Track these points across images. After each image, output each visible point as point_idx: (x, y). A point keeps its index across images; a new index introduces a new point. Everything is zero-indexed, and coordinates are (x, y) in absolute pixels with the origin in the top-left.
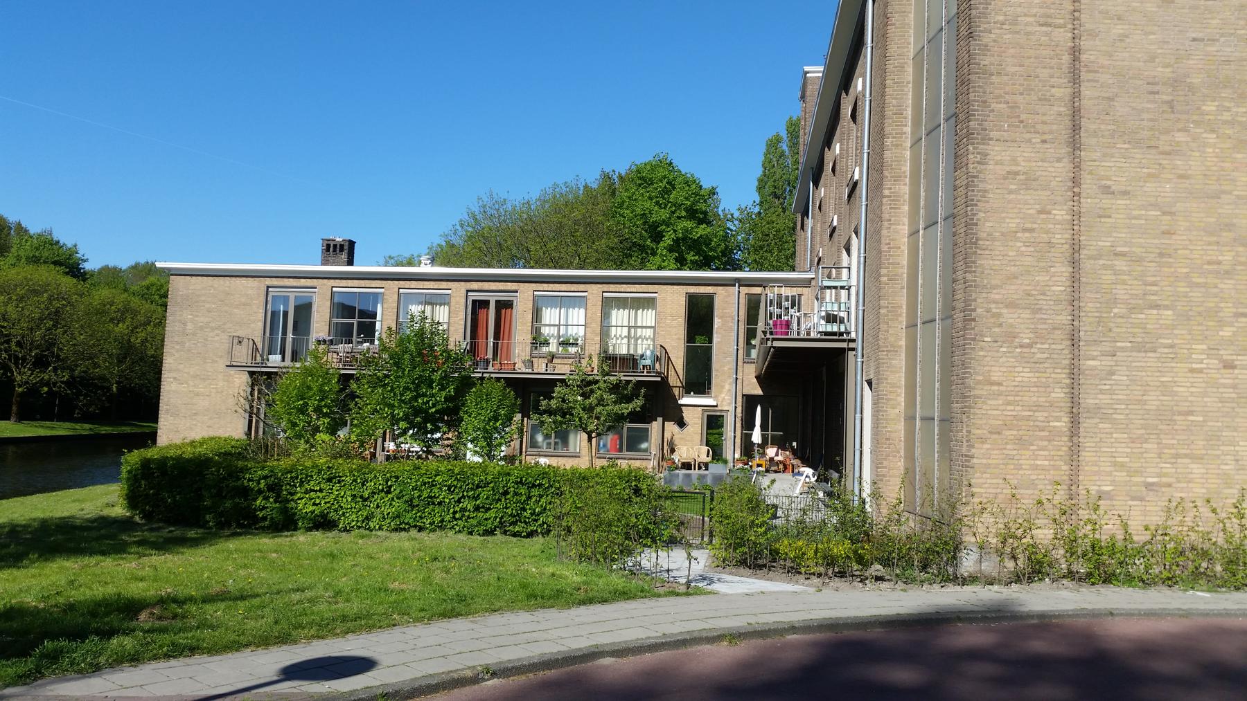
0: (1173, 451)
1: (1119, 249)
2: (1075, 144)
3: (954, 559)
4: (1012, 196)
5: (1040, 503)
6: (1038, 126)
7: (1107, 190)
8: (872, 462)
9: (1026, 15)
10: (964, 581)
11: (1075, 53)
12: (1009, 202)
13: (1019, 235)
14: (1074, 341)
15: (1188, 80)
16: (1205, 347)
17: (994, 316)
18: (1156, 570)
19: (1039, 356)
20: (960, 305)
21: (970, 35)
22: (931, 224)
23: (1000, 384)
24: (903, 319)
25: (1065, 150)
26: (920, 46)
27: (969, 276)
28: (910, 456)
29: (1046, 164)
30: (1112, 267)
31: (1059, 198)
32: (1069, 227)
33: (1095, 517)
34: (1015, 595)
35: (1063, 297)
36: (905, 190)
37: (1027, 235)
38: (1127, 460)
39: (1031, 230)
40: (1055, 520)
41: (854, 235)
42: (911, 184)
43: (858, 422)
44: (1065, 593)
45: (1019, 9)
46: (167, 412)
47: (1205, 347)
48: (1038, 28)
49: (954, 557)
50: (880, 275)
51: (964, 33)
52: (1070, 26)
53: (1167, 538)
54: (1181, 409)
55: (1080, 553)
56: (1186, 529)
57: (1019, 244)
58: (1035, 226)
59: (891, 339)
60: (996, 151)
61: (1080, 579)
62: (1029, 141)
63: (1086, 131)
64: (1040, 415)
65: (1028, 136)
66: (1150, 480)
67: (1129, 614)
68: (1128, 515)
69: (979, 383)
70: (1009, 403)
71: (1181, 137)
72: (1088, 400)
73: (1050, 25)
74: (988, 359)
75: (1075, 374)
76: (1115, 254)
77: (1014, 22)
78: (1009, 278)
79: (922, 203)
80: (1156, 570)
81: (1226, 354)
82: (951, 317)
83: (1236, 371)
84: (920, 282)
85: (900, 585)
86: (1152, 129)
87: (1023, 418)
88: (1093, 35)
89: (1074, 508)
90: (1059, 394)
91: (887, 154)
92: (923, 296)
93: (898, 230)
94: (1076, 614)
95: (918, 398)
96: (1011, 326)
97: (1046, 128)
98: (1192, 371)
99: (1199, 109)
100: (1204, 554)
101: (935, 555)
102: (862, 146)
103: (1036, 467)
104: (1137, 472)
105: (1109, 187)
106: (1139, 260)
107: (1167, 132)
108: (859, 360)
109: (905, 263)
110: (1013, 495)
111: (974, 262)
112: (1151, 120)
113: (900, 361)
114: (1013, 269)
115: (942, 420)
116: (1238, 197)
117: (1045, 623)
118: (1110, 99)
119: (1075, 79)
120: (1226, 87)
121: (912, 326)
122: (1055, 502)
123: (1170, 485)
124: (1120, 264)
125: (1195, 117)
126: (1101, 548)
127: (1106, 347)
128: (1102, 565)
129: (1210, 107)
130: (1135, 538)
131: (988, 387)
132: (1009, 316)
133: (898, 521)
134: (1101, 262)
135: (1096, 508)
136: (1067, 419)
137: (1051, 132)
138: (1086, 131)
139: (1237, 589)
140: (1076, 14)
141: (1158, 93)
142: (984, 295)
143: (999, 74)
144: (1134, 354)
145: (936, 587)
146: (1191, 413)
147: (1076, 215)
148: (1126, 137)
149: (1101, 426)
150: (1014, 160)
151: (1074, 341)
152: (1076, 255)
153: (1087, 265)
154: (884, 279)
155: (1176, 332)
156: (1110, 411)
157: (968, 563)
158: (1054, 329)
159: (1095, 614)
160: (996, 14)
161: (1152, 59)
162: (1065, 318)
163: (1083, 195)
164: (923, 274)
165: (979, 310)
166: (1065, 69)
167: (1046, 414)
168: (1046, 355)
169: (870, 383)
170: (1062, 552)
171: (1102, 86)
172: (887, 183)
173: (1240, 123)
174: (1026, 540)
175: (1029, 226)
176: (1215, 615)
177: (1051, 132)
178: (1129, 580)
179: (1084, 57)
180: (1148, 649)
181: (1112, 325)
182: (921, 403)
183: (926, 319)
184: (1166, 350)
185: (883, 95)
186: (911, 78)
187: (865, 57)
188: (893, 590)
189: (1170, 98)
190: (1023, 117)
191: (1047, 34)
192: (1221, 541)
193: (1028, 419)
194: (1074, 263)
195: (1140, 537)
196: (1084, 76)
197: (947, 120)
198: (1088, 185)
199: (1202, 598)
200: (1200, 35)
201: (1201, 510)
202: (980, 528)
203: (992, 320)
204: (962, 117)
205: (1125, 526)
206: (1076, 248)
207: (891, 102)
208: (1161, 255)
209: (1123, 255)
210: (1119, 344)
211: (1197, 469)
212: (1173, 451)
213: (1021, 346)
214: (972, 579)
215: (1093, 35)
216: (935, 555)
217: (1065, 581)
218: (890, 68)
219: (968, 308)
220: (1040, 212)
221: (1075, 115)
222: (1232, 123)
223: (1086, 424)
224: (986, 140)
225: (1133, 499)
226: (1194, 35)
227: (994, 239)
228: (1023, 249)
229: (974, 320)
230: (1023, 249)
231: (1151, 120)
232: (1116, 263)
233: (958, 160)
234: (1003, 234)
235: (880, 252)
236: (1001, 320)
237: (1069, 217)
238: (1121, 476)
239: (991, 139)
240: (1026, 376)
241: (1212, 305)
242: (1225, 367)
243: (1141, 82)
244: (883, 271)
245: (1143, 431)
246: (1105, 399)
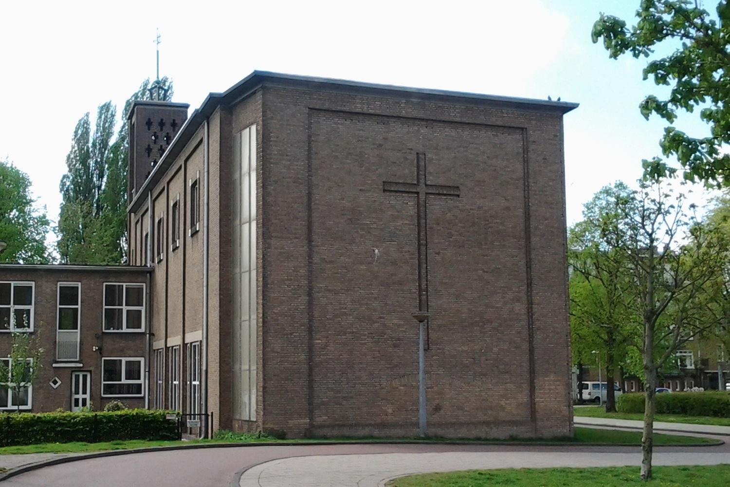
2: (310, 240)
98: (361, 344)
141: (345, 214)
238: (331, 393)
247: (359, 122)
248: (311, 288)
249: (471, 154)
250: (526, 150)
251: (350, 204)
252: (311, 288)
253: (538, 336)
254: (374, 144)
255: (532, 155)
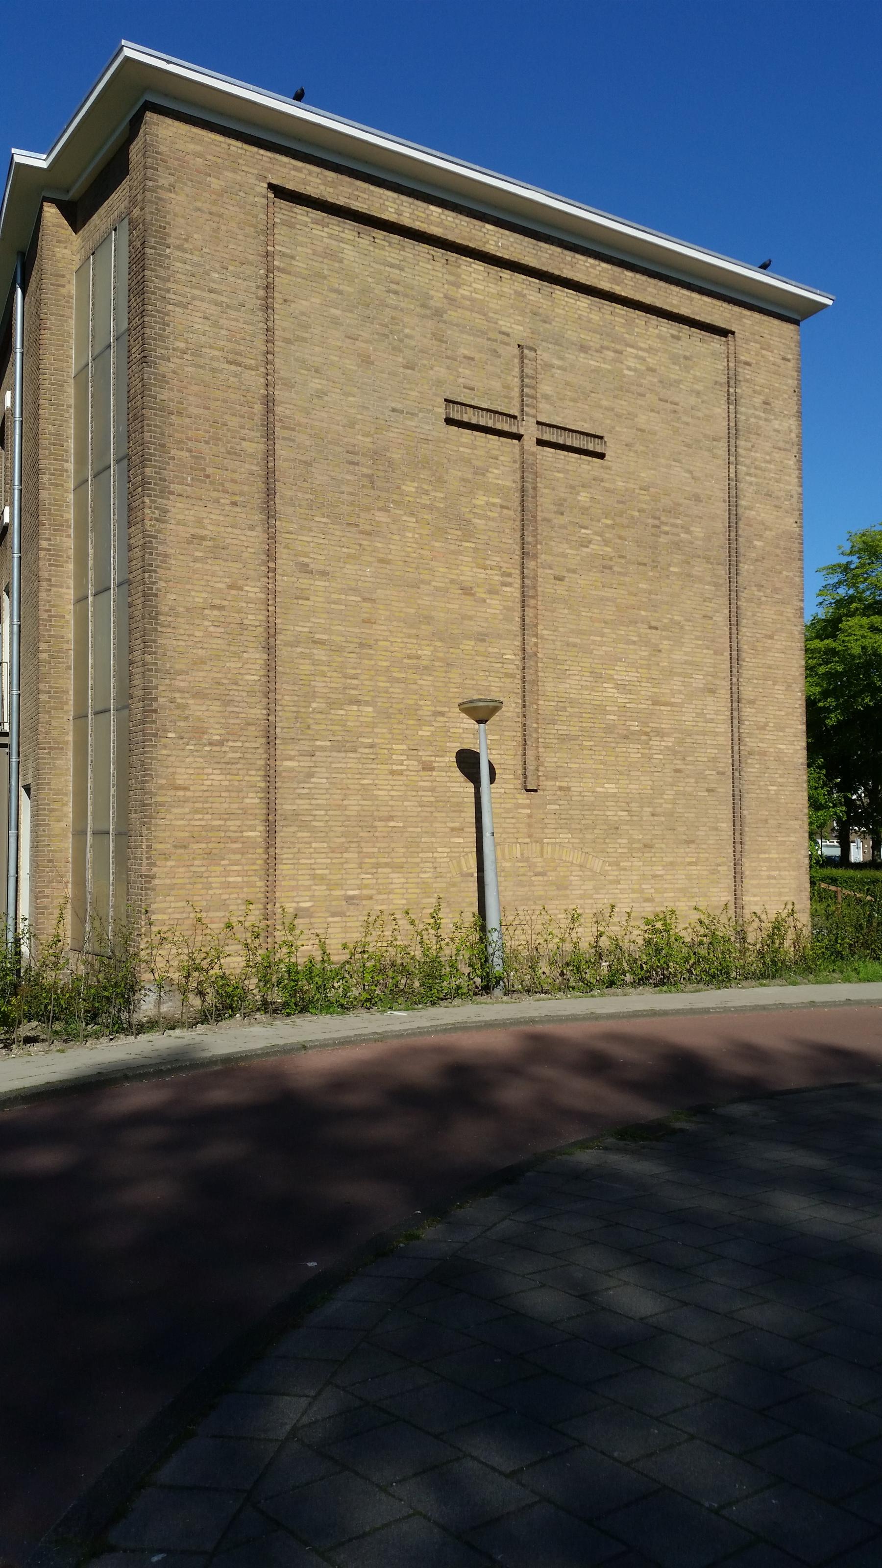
0: (374, 860)
1: (317, 636)
2: (269, 512)
3: (128, 1004)
4: (198, 565)
5: (229, 926)
6: (227, 485)
7: (304, 568)
8: (31, 891)
9: (211, 347)
10: (141, 1029)
11: (269, 403)
12: (195, 572)
13: (206, 612)
14: (270, 739)
15: (388, 454)
16: (404, 747)
17: (180, 707)
18: (355, 992)
19: (231, 755)
20: (138, 693)
21: (144, 360)
22: (102, 590)
23: (186, 789)
24: (70, 707)
25: (258, 517)
26: (83, 363)
27: (148, 657)
28: (80, 882)
29: (236, 531)
30: (310, 657)
31: (252, 573)
32: (263, 607)
33: (291, 938)
34: (198, 1039)
35: (257, 688)
36: (69, 543)
37: (216, 612)
38: (327, 871)
39: (221, 608)
40: (247, 945)
41: (5, 596)
42: (76, 537)
43: (13, 840)
44: (256, 1030)
45: (203, 338)
46: (472, 904)
47: (404, 747)
48: (226, 366)
49: (128, 1002)
50: (38, 650)
51: (136, 355)
52: (263, 370)
53: (366, 956)
54: (381, 814)
55: (274, 979)
56: (385, 944)
57: (207, 623)
58: (226, 603)
59: (55, 733)
60: (177, 508)
61: (275, 1011)
62: (217, 501)
63: (282, 498)
64: (233, 824)
65: (215, 494)
66: (351, 893)
67: (323, 1045)
68: (326, 932)
69: (161, 787)
70: (197, 811)
71: (381, 517)
72: (285, 806)
73: (240, 365)
74: (171, 759)
75: (271, 776)
76: (314, 642)
77: (197, 353)
78: (195, 664)
79: (91, 563)
80: (355, 992)
81: (425, 755)
82: (128, 707)
83: (434, 773)
84: (90, 661)
85: (58, 1045)
86: (352, 504)
87: (213, 829)
88: (289, 385)
89: (269, 931)
90: (253, 800)
91: (44, 495)
92: (94, 679)
93: (62, 594)
94: (267, 1053)
95: (90, 808)
96: (199, 719)
97: (236, 488)
98: (392, 773)
99: (399, 488)
100: (404, 971)
101: (108, 1002)
102: (12, 480)
103: (227, 885)
104: (339, 885)
105: (307, 565)
106: (339, 650)
107: (367, 509)
108: (14, 760)
109: (71, 636)
110: (199, 920)
111: (155, 641)
112: (351, 494)
113: (67, 761)
114: (201, 652)
115: (118, 834)
116: (437, 589)
117: (230, 1067)
118: (308, 464)
119: (269, 435)
120: (424, 467)
121: (80, 717)
122: (247, 924)
123: (371, 898)
124: (320, 654)
125: (395, 497)
126: (297, 973)
127: (305, 745)
128: (300, 991)
129: (409, 487)
130: (334, 958)
131: (172, 793)
132: (197, 708)
133: (56, 964)
134: (299, 650)
135: (292, 928)
136: (261, 828)
137: (241, 494)
138: (282, 498)
139: (433, 1004)
140: (270, 357)
141: (357, 464)
142: (167, 682)
143: (180, 414)
144: (335, 754)
145: (104, 1040)
146: (391, 818)
147: (271, 593)
148: (325, 510)
149: (300, 834)
150: (199, 522)
151: (270, 739)
152: (272, 640)
153: (283, 652)
154: (44, 656)
155: (376, 730)
156: (310, 818)
157: (147, 1006)
158: (248, 724)
159: (287, 1050)
160: (176, 339)
161: (352, 424)
162: (259, 712)
163: (279, 571)
164: (94, 652)
165: (161, 700)
166: (258, 419)
167: (238, 823)
168: (238, 755)
169: (28, 789)
170: (255, 981)
171: (298, 448)
172: (45, 532)
173: (438, 508)
174: (215, 971)
175: (218, 602)
176: (409, 1035)
177: (241, 494)
178: (328, 1007)
179: (278, 410)
180: (341, 1082)
181: (311, 721)
182: (94, 813)
183: (99, 708)
184: (367, 750)
185: (37, 417)
186: (72, 402)
187: (14, 364)
188: (47, 1052)
189: (370, 472)
190: (210, 471)
191: (236, 375)
192: (418, 954)
193: (219, 829)
194: (270, 649)
195: (338, 957)
196: (279, 432)
197: (118, 461)
198: (284, 561)
199: (399, 1017)
200: (399, 406)
201: (400, 922)
202: (164, 961)
203: (177, 712)
204: (135, 460)
205: (323, 946)
206: (272, 631)
207: (47, 428)
208: (362, 645)
209: (322, 642)
210: (318, 743)
211: (397, 878)
212: (374, 860)
213: (210, 744)
214: (152, 1025)
215: (289, 385)
216: (108, 1002)
217: (258, 1016)
218: (45, 384)
219: (147, 697)
220: (230, 587)
221: (270, 476)
222: (431, 508)
223: (284, 833)
224: (165, 493)
225: (334, 915)
226: (393, 405)
227: (177, 615)
228: (212, 629)
229: (155, 711)
230: (212, 629)
231: (351, 494)
232: (315, 651)
233: (132, 514)
234: (188, 610)
235: (38, 621)
236: (187, 712)
237: (263, 596)
238: (320, 890)
239: (172, 493)
240: (216, 778)
241: (411, 702)
242: (424, 769)
243: (340, 449)
244: (43, 646)
245: (343, 840)
246: (303, 804)
247: (390, 246)
248: (271, 632)
249: (629, 368)
250: (732, 380)
251: (368, 440)
252: (271, 632)
253: (752, 768)
254: (423, 306)
255: (743, 390)
